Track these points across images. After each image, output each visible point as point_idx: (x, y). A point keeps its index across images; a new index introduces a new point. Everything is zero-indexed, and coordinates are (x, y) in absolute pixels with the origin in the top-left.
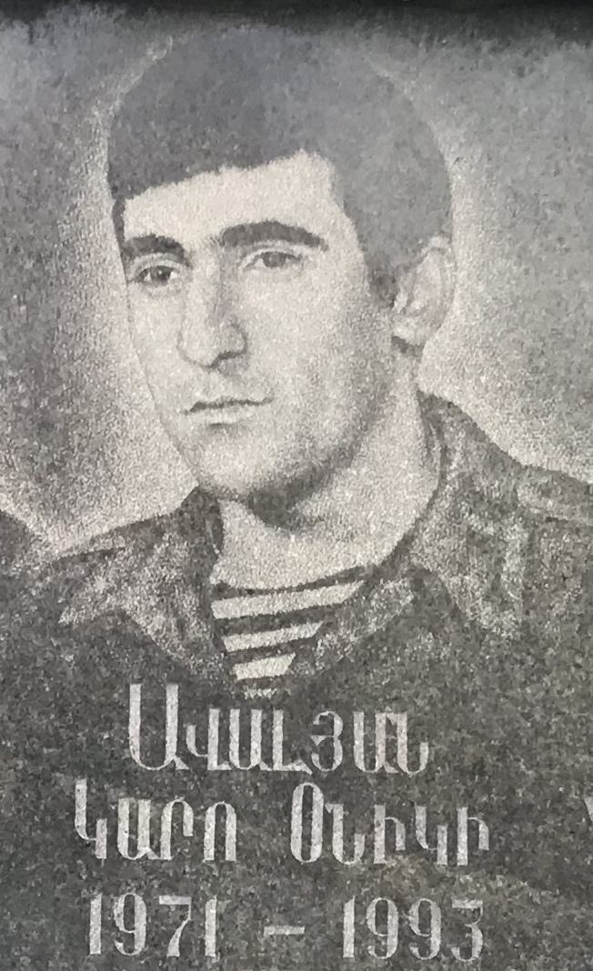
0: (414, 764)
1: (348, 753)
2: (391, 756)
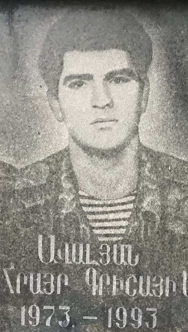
0: (133, 262)
1: (112, 260)
2: (126, 259)
